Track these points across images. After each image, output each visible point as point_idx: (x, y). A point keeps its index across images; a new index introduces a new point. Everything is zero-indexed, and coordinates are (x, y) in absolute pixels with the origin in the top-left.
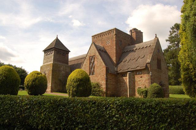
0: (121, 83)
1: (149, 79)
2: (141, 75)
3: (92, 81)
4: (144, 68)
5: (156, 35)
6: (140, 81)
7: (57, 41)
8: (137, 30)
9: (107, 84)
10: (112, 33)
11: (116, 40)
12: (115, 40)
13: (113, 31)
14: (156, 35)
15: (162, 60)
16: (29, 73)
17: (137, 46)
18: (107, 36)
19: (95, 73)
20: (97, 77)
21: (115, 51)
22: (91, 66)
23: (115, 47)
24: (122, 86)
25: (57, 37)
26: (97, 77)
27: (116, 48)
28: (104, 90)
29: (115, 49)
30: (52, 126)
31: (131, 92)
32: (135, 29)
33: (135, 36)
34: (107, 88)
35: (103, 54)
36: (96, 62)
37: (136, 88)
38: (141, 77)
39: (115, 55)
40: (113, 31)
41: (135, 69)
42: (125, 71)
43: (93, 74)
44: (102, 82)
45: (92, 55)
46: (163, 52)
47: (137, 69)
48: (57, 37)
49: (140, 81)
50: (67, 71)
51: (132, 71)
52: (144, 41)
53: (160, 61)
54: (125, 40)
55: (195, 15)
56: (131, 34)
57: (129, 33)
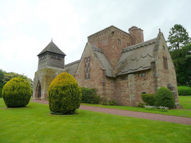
5: (160, 30)
6: (143, 84)
8: (137, 27)
14: (160, 30)
15: (168, 59)
16: (31, 76)
18: (103, 35)
25: (52, 41)
36: (91, 65)
41: (137, 70)
44: (99, 88)
47: (139, 70)
48: (52, 41)
49: (143, 84)
53: (167, 59)
54: (124, 39)
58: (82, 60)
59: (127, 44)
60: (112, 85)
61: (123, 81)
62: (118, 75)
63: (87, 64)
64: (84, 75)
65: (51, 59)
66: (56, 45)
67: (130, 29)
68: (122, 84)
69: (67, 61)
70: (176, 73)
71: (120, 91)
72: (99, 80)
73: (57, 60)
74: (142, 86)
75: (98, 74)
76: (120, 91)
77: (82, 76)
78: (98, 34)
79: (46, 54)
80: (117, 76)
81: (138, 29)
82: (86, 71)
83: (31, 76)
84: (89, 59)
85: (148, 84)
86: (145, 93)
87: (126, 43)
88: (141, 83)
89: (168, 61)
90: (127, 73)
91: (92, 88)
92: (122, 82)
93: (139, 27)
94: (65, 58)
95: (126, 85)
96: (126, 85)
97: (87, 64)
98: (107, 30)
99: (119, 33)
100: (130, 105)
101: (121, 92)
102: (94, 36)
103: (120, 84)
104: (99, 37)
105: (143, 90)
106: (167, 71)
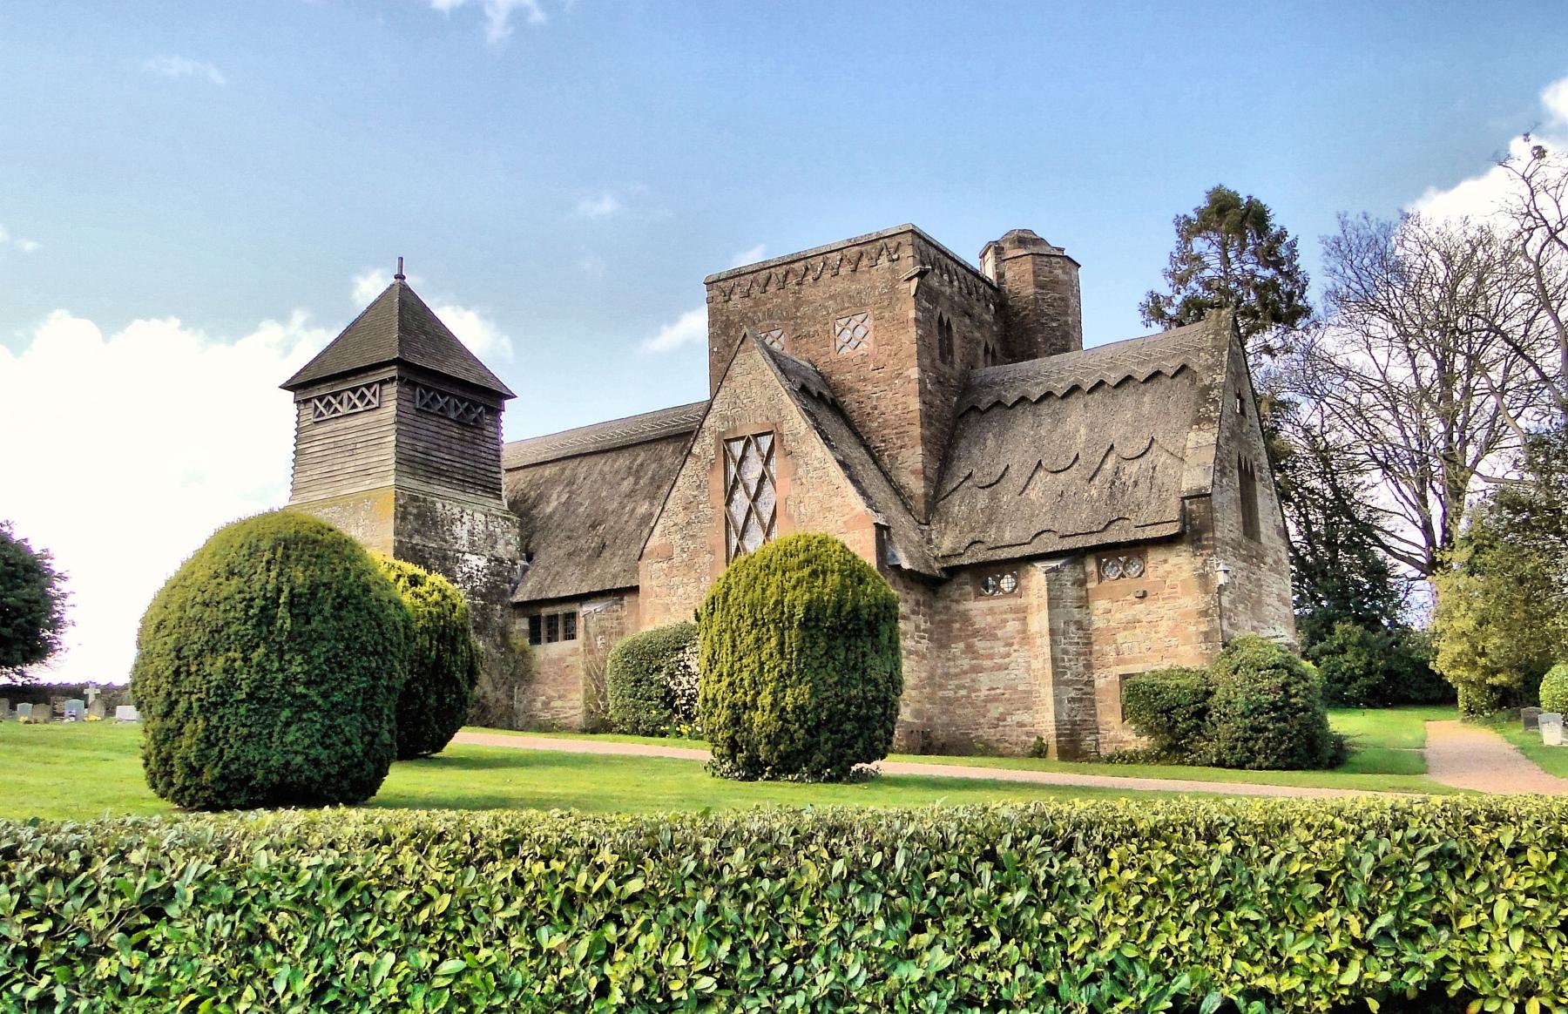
0: (979, 645)
4: (1172, 529)
6: (1133, 623)
7: (407, 310)
10: (884, 261)
12: (912, 314)
13: (892, 244)
17: (1050, 371)
18: (839, 286)
22: (739, 514)
23: (914, 373)
24: (987, 663)
25: (400, 277)
32: (1023, 239)
35: (825, 416)
37: (1106, 680)
40: (892, 244)
41: (1094, 541)
45: (748, 432)
46: (854, 768)
49: (1133, 623)
50: (500, 550)
51: (1075, 556)
55: (996, 1004)
56: (1000, 276)
59: (981, 352)
60: (917, 628)
61: (993, 603)
62: (955, 562)
65: (422, 422)
68: (980, 623)
69: (522, 428)
71: (965, 663)
73: (455, 432)
76: (965, 663)
79: (382, 383)
80: (953, 572)
81: (1046, 250)
83: (1546, 742)
84: (765, 442)
85: (1164, 627)
87: (978, 343)
88: (1118, 616)
89: (1259, 486)
90: (1028, 550)
92: (978, 608)
93: (1040, 235)
94: (503, 416)
95: (1012, 626)
96: (1012, 626)
99: (946, 277)
100: (1018, 756)
101: (977, 669)
103: (966, 618)
104: (808, 291)
106: (1254, 545)
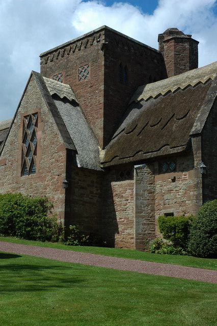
1: (196, 186)
2: (172, 175)
3: (157, 176)
4: (180, 149)
8: (181, 33)
9: (68, 202)
11: (105, 65)
13: (98, 35)
18: (82, 53)
19: (37, 167)
20: (43, 179)
21: (102, 100)
23: (102, 87)
26: (43, 179)
27: (105, 91)
28: (61, 221)
29: (103, 92)
30: (187, 202)
31: (141, 226)
33: (172, 54)
34: (68, 215)
36: (39, 134)
38: (174, 180)
39: (102, 111)
41: (155, 154)
42: (127, 160)
43: (31, 171)
44: (56, 197)
45: (30, 113)
47: (160, 153)
49: (170, 191)
52: (200, 65)
56: (162, 48)
57: (155, 45)
58: (18, 121)
63: (30, 132)
64: (20, 162)
66: (88, 32)
67: (161, 38)
70: (176, 171)
72: (57, 177)
74: (166, 197)
75: (54, 160)
77: (15, 164)
78: (68, 48)
82: (25, 150)
85: (181, 192)
86: (172, 214)
88: (165, 187)
91: (38, 197)
97: (30, 132)
98: (90, 39)
102: (56, 54)
105: (168, 208)
